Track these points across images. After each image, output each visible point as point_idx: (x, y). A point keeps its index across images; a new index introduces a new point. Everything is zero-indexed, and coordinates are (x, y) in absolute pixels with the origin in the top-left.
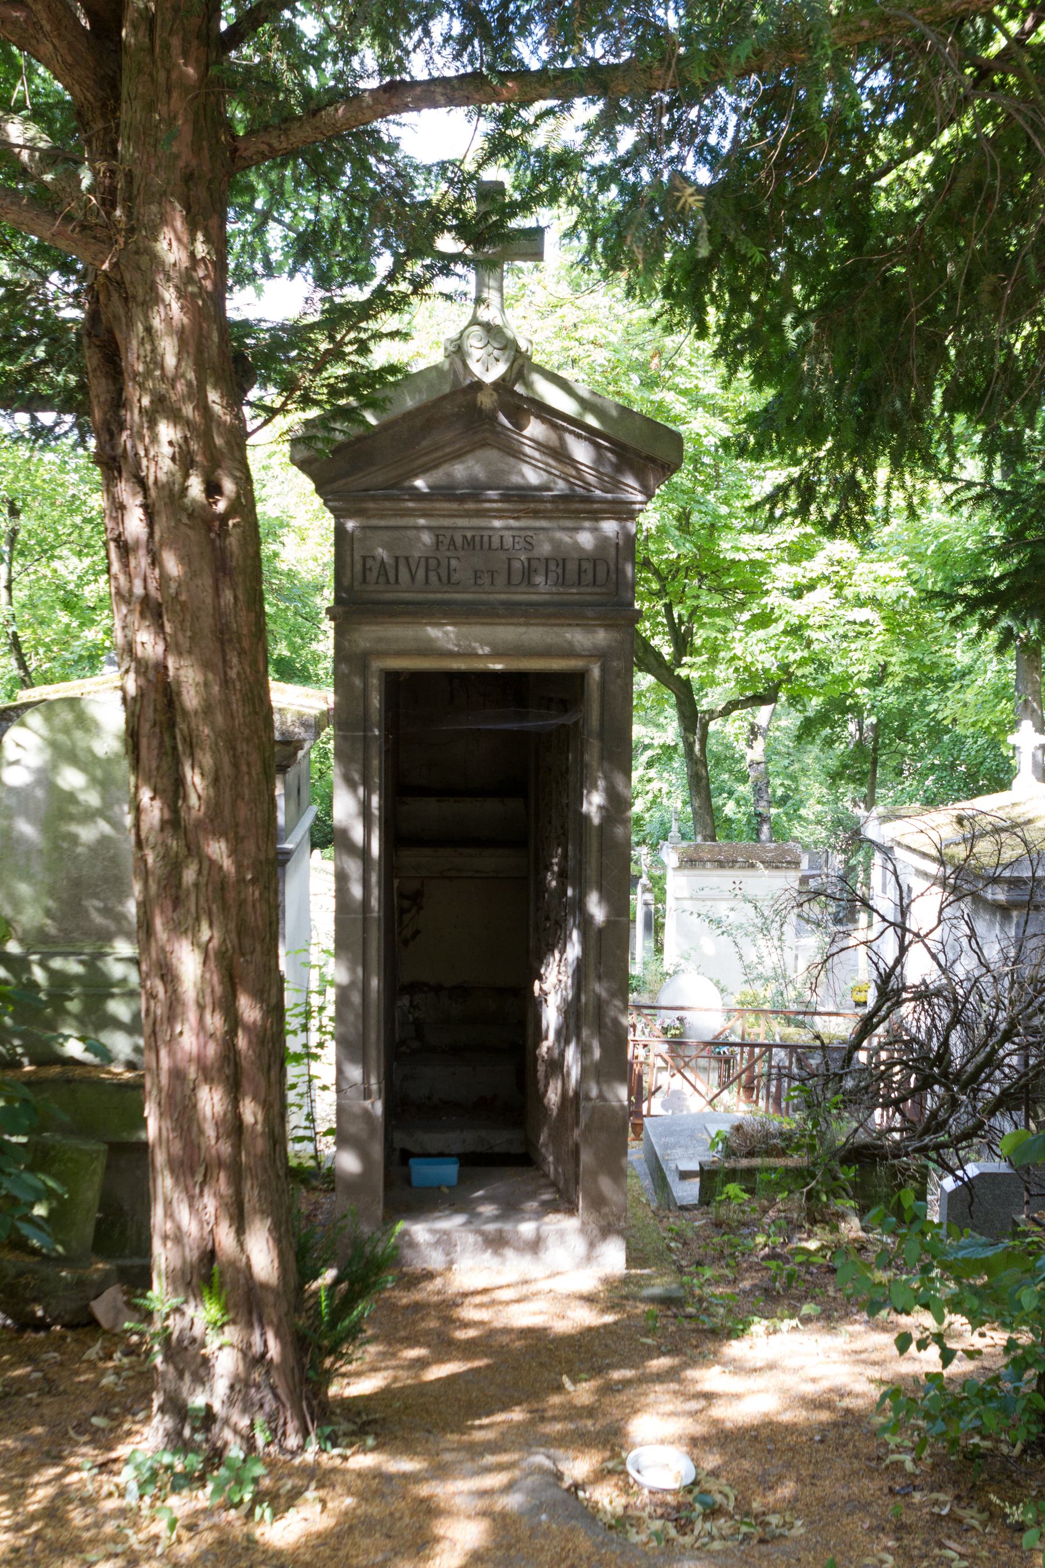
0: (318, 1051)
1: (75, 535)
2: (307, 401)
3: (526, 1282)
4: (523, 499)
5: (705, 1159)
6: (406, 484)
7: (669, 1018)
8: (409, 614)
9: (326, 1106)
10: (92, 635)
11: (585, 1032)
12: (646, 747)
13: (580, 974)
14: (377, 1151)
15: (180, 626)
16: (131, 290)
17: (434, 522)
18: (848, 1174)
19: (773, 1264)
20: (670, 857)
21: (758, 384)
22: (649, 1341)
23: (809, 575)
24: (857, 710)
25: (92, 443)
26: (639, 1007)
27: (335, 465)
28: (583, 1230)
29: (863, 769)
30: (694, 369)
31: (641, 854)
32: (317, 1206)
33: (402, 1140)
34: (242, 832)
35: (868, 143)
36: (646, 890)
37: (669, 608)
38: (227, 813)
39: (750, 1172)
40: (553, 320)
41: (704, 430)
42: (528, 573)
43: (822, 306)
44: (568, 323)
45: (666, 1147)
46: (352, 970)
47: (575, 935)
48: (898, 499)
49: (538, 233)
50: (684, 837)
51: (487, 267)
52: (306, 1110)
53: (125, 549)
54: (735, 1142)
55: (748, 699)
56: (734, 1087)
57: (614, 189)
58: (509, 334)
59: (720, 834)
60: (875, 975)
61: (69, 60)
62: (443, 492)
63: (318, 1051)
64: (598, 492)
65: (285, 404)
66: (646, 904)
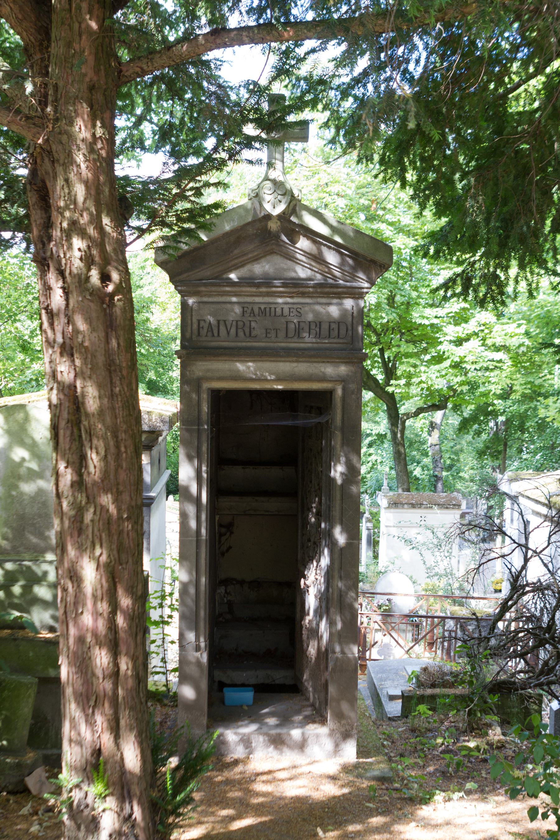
0: (170, 620)
1: (29, 307)
2: (164, 224)
3: (295, 767)
4: (296, 286)
5: (404, 688)
6: (225, 276)
7: (382, 600)
8: (225, 355)
9: (173, 653)
10: (36, 366)
11: (332, 610)
12: (368, 435)
13: (329, 575)
14: (204, 685)
15: (85, 361)
16: (56, 155)
17: (242, 299)
18: (493, 699)
19: (447, 756)
20: (382, 501)
21: (438, 214)
22: (371, 805)
23: (466, 332)
24: (495, 414)
25: (32, 249)
26: (364, 593)
27: (180, 265)
28: (331, 734)
29: (498, 450)
30: (397, 210)
31: (366, 499)
32: (167, 716)
33: (219, 675)
34: (121, 488)
35: (506, 71)
36: (369, 520)
37: (382, 351)
38: (112, 477)
39: (433, 697)
40: (314, 181)
41: (403, 245)
42: (298, 332)
43: (478, 168)
44: (323, 182)
45: (381, 680)
46: (190, 573)
47: (326, 551)
48: (523, 286)
49: (304, 124)
50: (391, 489)
51: (275, 144)
52: (161, 656)
53: (51, 315)
54: (423, 678)
55: (429, 407)
56: (422, 643)
57: (351, 99)
58: (288, 186)
59: (413, 487)
60: (507, 575)
61: (20, 16)
62: (247, 282)
63: (170, 620)
64: (341, 282)
65: (150, 226)
66: (368, 529)
